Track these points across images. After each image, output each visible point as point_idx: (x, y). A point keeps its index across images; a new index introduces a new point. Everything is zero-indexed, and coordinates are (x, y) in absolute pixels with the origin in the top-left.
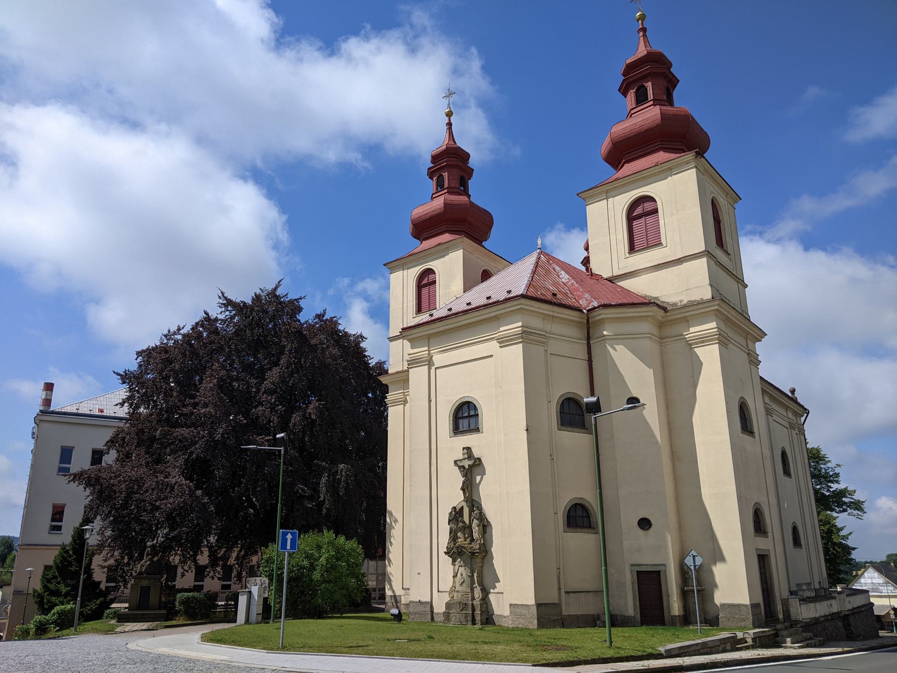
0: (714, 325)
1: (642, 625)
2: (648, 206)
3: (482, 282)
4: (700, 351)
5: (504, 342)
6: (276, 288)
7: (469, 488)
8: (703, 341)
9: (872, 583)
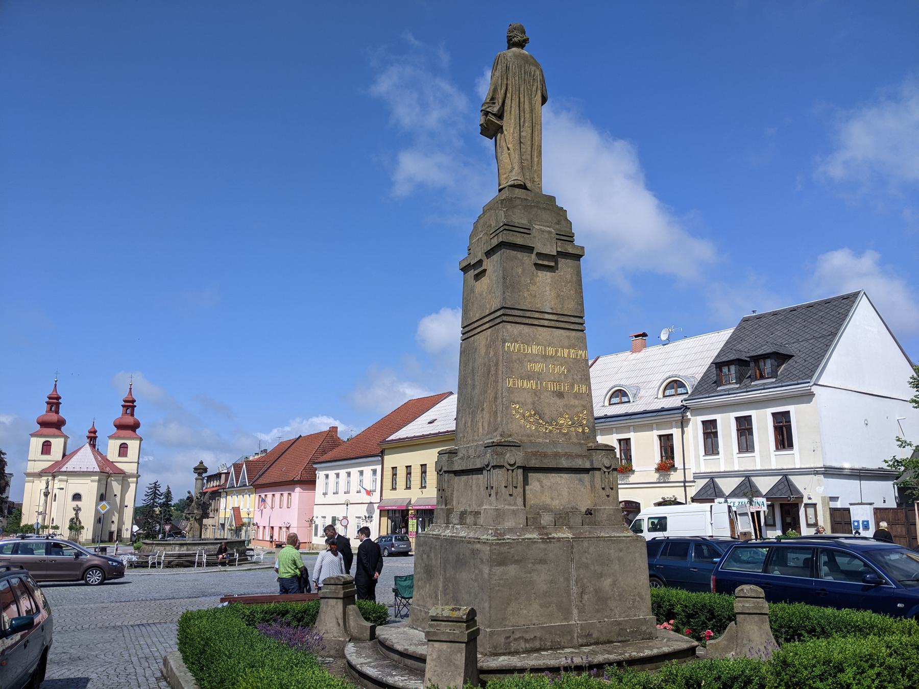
0: (97, 478)
3: (649, 564)
4: (131, 484)
5: (92, 481)
6: (683, 433)
7: (77, 514)
8: (133, 483)
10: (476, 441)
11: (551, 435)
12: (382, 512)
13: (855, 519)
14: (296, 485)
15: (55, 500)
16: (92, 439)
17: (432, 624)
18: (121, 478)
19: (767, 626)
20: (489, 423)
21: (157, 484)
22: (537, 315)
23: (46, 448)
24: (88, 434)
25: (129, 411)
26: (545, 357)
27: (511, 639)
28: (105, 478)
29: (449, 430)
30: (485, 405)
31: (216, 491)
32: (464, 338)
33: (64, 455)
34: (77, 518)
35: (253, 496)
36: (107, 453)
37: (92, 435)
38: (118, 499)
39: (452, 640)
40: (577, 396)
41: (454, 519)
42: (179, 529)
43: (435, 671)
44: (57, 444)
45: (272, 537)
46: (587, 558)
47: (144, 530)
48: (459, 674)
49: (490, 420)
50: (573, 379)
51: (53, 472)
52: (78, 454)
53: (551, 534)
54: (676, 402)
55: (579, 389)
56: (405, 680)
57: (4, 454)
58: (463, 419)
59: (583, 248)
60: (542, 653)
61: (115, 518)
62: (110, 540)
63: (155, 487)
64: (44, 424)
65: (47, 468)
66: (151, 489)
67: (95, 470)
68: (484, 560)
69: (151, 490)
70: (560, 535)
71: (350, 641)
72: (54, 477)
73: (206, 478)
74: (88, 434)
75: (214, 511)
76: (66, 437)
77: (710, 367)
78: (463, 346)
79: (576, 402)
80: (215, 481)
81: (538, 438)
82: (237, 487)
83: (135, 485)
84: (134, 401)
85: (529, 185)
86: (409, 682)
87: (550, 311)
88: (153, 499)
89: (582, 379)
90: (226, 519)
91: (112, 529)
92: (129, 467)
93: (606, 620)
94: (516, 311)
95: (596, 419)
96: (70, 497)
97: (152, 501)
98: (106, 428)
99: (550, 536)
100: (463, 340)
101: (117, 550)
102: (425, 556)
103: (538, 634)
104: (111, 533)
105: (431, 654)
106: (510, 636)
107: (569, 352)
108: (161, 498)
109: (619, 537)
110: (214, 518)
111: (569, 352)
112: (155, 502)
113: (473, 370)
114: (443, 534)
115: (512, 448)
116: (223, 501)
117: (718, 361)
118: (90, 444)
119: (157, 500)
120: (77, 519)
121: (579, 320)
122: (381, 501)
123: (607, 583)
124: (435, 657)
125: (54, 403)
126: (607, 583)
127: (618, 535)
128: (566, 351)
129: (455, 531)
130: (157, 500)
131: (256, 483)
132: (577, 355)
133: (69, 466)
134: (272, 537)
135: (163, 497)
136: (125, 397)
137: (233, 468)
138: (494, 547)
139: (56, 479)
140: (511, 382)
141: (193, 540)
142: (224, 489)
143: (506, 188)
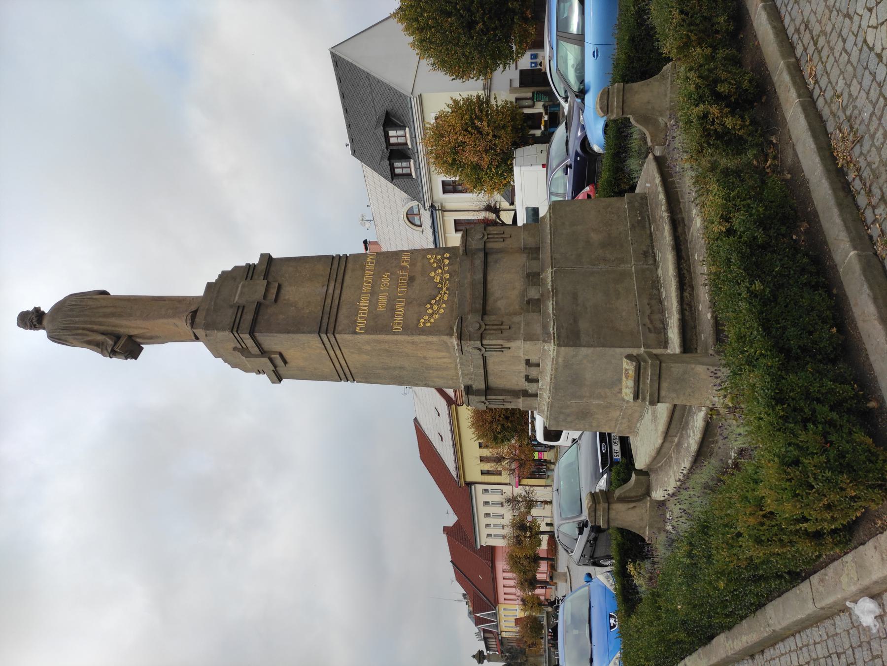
10: (456, 365)
11: (451, 289)
13: (529, 65)
17: (642, 398)
19: (636, 85)
20: (438, 350)
22: (329, 301)
26: (373, 293)
27: (650, 326)
29: (448, 421)
30: (421, 355)
32: (352, 379)
39: (658, 376)
40: (413, 264)
41: (533, 389)
43: (690, 395)
46: (572, 255)
48: (692, 369)
49: (436, 350)
50: (396, 267)
53: (549, 289)
54: (426, 216)
55: (406, 261)
56: (694, 432)
58: (435, 380)
59: (262, 256)
60: (664, 297)
68: (574, 353)
70: (550, 279)
71: (650, 497)
73: (488, 652)
77: (395, 185)
78: (360, 380)
79: (419, 264)
81: (454, 301)
85: (193, 308)
86: (696, 427)
87: (325, 288)
89: (396, 259)
93: (630, 238)
94: (324, 321)
95: (436, 247)
99: (550, 290)
100: (354, 380)
102: (569, 419)
103: (646, 301)
105: (672, 399)
106: (648, 328)
107: (369, 270)
109: (550, 225)
111: (369, 270)
113: (385, 369)
114: (547, 400)
115: (464, 325)
117: (390, 176)
121: (336, 262)
123: (595, 237)
124: (675, 395)
126: (595, 237)
127: (549, 226)
128: (367, 273)
129: (545, 387)
132: (371, 263)
137: (480, 626)
138: (561, 343)
140: (397, 327)
141: (546, 663)
143: (194, 330)
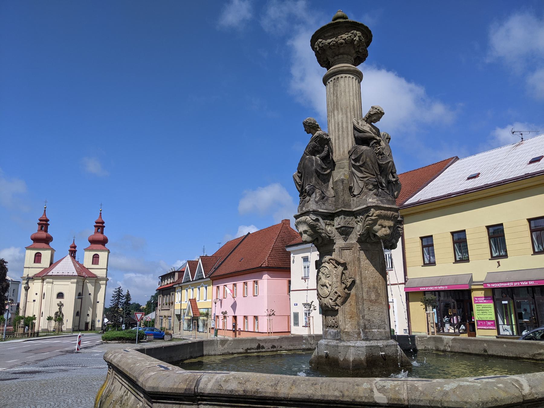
0: (76, 280)
1: (203, 341)
2: (39, 254)
4: (101, 286)
7: (60, 309)
8: (103, 284)
9: (437, 350)
12: (410, 295)
14: (264, 272)
15: (44, 298)
16: (73, 253)
18: (94, 281)
21: (121, 289)
23: (38, 258)
24: (69, 248)
25: (99, 230)
28: (82, 280)
31: (171, 286)
33: (51, 264)
34: (61, 312)
35: (210, 288)
36: (83, 262)
37: (73, 249)
38: (92, 297)
42: (135, 321)
44: (46, 255)
45: (235, 326)
47: (112, 322)
51: (43, 276)
52: (62, 262)
57: (6, 262)
61: (90, 312)
62: (86, 329)
63: (119, 291)
64: (36, 240)
65: (38, 274)
66: (117, 292)
67: (74, 274)
69: (116, 293)
72: (43, 280)
74: (69, 248)
75: (169, 304)
76: (53, 250)
80: (169, 280)
82: (193, 281)
83: (104, 286)
84: (103, 223)
88: (118, 300)
90: (182, 310)
91: (88, 321)
92: (101, 273)
96: (55, 296)
97: (117, 301)
98: (82, 244)
101: (79, 343)
104: (87, 324)
108: (123, 298)
110: (169, 310)
112: (119, 301)
116: (178, 296)
118: (71, 256)
119: (121, 300)
120: (60, 313)
122: (406, 281)
125: (44, 224)
130: (121, 300)
131: (213, 275)
133: (55, 271)
134: (235, 326)
135: (124, 298)
136: (97, 219)
137: (187, 265)
139: (45, 281)
142: (179, 284)
